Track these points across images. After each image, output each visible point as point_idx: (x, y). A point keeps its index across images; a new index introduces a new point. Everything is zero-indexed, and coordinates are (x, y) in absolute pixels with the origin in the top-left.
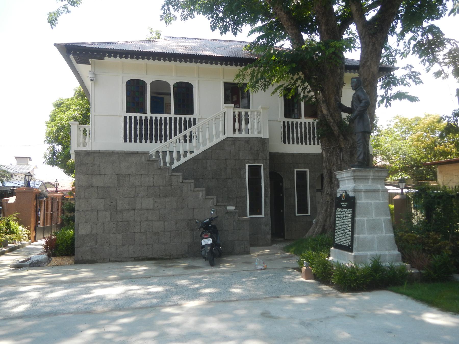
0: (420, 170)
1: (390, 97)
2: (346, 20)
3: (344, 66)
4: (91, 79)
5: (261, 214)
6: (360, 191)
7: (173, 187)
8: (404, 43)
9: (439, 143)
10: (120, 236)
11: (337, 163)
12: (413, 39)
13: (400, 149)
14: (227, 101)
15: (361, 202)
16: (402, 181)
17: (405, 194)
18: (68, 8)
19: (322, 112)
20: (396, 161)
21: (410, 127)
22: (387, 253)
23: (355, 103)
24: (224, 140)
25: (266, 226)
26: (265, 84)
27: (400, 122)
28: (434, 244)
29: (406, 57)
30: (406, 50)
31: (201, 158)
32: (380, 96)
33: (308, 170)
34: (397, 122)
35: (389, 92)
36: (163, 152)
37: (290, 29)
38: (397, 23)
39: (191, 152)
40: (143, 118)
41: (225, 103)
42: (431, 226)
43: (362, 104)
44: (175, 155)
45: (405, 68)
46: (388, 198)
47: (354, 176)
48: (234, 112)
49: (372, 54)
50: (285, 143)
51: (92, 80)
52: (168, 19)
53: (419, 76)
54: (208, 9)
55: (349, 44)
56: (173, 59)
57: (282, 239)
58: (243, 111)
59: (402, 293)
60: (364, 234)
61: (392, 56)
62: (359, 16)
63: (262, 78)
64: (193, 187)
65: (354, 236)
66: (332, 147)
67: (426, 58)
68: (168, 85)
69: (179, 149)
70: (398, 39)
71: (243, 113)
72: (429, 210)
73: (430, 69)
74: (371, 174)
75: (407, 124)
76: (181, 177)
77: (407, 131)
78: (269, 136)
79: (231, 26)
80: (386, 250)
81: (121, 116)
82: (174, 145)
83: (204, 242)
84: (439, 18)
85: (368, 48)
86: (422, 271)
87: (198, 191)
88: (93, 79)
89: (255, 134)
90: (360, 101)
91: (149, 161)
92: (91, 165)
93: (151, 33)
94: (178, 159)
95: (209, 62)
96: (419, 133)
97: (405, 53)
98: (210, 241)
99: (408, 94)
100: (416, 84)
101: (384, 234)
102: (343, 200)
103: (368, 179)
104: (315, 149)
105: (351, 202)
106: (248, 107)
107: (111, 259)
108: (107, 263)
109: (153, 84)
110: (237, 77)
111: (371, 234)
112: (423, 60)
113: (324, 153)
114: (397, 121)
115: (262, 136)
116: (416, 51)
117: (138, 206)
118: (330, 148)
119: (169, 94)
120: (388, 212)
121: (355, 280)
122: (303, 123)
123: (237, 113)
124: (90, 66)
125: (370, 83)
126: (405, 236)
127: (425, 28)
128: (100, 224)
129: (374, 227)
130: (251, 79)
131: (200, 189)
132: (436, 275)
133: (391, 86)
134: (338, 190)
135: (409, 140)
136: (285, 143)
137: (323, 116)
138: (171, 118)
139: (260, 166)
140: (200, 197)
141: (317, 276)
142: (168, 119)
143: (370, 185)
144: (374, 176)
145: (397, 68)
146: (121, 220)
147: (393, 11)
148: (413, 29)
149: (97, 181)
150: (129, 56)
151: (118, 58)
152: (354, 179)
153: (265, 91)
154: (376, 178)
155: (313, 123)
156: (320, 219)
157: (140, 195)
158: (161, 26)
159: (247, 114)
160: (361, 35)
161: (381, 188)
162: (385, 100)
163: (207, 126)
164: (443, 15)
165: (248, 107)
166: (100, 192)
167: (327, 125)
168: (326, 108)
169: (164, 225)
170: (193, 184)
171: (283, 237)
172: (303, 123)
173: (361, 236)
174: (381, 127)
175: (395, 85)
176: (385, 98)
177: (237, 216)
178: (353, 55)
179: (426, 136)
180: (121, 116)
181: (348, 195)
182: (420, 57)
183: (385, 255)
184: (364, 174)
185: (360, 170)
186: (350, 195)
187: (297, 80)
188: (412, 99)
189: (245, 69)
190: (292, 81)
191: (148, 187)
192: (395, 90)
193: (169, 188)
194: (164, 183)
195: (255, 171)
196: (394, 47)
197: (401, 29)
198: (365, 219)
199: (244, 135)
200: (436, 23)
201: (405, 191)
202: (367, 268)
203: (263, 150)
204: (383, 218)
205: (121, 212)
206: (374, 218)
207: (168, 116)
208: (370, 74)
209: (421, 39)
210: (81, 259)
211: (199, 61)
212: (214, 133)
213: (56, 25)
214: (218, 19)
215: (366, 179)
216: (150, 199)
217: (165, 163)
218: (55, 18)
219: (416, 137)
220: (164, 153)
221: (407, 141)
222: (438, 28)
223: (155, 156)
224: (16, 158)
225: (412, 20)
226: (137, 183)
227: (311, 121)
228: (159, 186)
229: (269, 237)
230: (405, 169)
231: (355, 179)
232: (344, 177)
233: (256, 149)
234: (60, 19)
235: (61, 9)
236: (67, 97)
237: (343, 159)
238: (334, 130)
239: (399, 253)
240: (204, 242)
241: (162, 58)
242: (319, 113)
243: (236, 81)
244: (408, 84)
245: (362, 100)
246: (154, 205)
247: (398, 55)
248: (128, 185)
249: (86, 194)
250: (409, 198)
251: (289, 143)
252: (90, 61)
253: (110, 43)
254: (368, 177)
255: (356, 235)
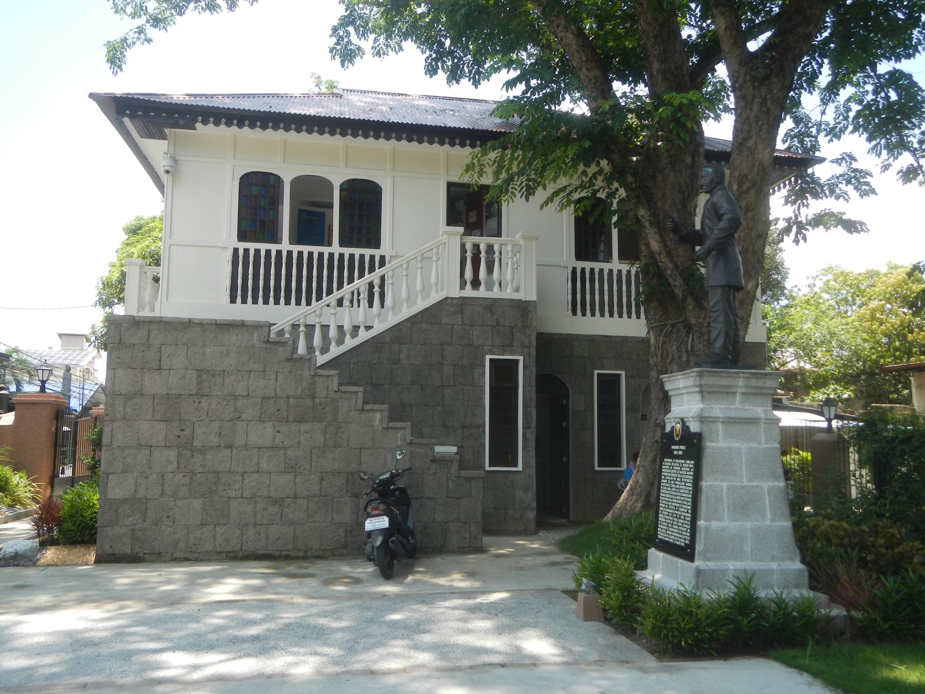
0: (875, 380)
1: (804, 221)
2: (709, 51)
3: (701, 150)
4: (166, 168)
5: (516, 466)
6: (714, 420)
7: (317, 400)
8: (836, 107)
9: (917, 326)
10: (197, 504)
11: (680, 357)
12: (855, 101)
13: (833, 334)
14: (453, 219)
15: (754, 445)
16: (828, 402)
17: (835, 430)
18: (147, 32)
19: (648, 245)
20: (827, 359)
21: (854, 289)
22: (774, 565)
23: (707, 222)
24: (440, 303)
25: (525, 491)
26: (528, 187)
27: (835, 280)
28: (887, 548)
29: (839, 138)
30: (839, 123)
31: (388, 339)
32: (784, 219)
33: (623, 373)
34: (828, 281)
35: (803, 210)
36: (306, 326)
37: (584, 70)
38: (821, 66)
39: (368, 328)
40: (274, 254)
41: (449, 224)
42: (885, 505)
43: (722, 224)
44: (333, 333)
45: (838, 161)
46: (779, 438)
47: (700, 386)
48: (463, 246)
49: (760, 123)
50: (574, 313)
51: (167, 172)
52: (347, 54)
53: (869, 179)
54: (422, 33)
55: (714, 102)
56: (338, 130)
57: (564, 521)
58: (483, 242)
59: (801, 668)
60: (720, 519)
61: (810, 136)
62: (732, 41)
63: (521, 173)
64: (360, 401)
65: (699, 523)
66: (670, 322)
67: (883, 141)
68: (328, 185)
69: (346, 320)
70: (822, 100)
71: (483, 247)
72: (880, 468)
73: (890, 165)
74: (741, 382)
75: (850, 286)
76: (336, 380)
77: (850, 298)
78: (538, 296)
79: (468, 67)
80: (772, 560)
81: (226, 248)
82: (322, 312)
83: (371, 524)
84: (914, 55)
85: (751, 110)
86: (853, 613)
87: (372, 410)
88: (169, 169)
89: (508, 294)
90: (720, 217)
91: (268, 342)
92: (142, 348)
93: (317, 85)
94: (340, 341)
95: (415, 137)
96: (874, 304)
97: (837, 130)
98: (383, 522)
99: (844, 217)
100: (862, 197)
101: (768, 523)
102: (677, 439)
103: (734, 393)
104: (633, 327)
105: (693, 445)
106: (499, 235)
107: (175, 555)
108: (165, 562)
109: (296, 182)
110: (467, 171)
111: (738, 520)
112: (876, 146)
113: (651, 334)
114: (830, 277)
115: (521, 296)
116: (860, 126)
117: (239, 440)
118: (665, 325)
119: (331, 206)
120: (780, 471)
121: (691, 631)
122: (615, 273)
123: (469, 246)
124: (166, 142)
125: (754, 185)
126: (823, 527)
127: (884, 75)
128: (154, 476)
129: (745, 505)
130: (497, 173)
131: (376, 407)
132: (887, 625)
133: (807, 199)
134: (668, 416)
135: (853, 317)
136: (574, 313)
137: (652, 255)
138: (331, 255)
139: (517, 361)
140: (377, 423)
141: (609, 616)
142: (326, 256)
143: (738, 407)
144: (746, 387)
145: (822, 160)
146: (201, 470)
147: (807, 31)
148: (855, 79)
149: (153, 384)
150: (247, 122)
151: (223, 127)
152: (701, 392)
153: (527, 199)
154: (753, 391)
155: (629, 272)
156: (640, 481)
157: (244, 416)
158: (332, 70)
159: (490, 249)
160: (736, 81)
161: (762, 416)
162: (794, 229)
163: (404, 273)
164: (920, 48)
165: (499, 235)
166: (157, 408)
167: (660, 275)
168: (658, 238)
169: (295, 482)
170: (360, 396)
171: (566, 516)
172: (615, 273)
173: (715, 524)
174: (796, 290)
175: (816, 196)
176: (794, 223)
177: (455, 467)
178: (719, 129)
179: (891, 310)
180: (226, 248)
181: (688, 428)
182: (869, 140)
183: (769, 572)
184: (725, 382)
185: (715, 372)
186: (692, 430)
187: (594, 176)
188: (851, 226)
189: (485, 153)
190: (584, 178)
191: (263, 398)
192: (815, 206)
193: (309, 402)
194: (299, 392)
195: (504, 373)
196: (815, 116)
197: (830, 79)
198: (724, 485)
199: (482, 292)
200: (905, 66)
201: (835, 424)
202: (720, 602)
203: (524, 327)
204: (766, 485)
205: (203, 451)
206: (746, 483)
207: (326, 250)
208: (753, 166)
209: (872, 100)
210: (110, 552)
211: (393, 135)
212: (418, 287)
213: (124, 66)
214: (441, 54)
215: (729, 393)
216: (267, 425)
217: (310, 348)
218: (121, 53)
219: (868, 312)
220: (310, 328)
221: (850, 320)
222: (909, 77)
223: (291, 334)
224: (60, 335)
225: (852, 57)
226: (240, 390)
227: (625, 267)
228: (288, 397)
229: (532, 515)
230: (844, 379)
231: (704, 392)
232: (680, 389)
233: (508, 324)
234: (130, 54)
235: (131, 34)
236: (151, 215)
237: (692, 350)
238: (675, 286)
239: (802, 566)
240: (371, 524)
241: (316, 128)
242: (643, 248)
243: (466, 179)
244: (845, 196)
245: (722, 215)
246: (274, 438)
247: (822, 134)
248: (220, 393)
249: (129, 410)
250: (844, 440)
251: (584, 314)
252: (167, 131)
253: (206, 96)
254: (734, 390)
255: (702, 522)
